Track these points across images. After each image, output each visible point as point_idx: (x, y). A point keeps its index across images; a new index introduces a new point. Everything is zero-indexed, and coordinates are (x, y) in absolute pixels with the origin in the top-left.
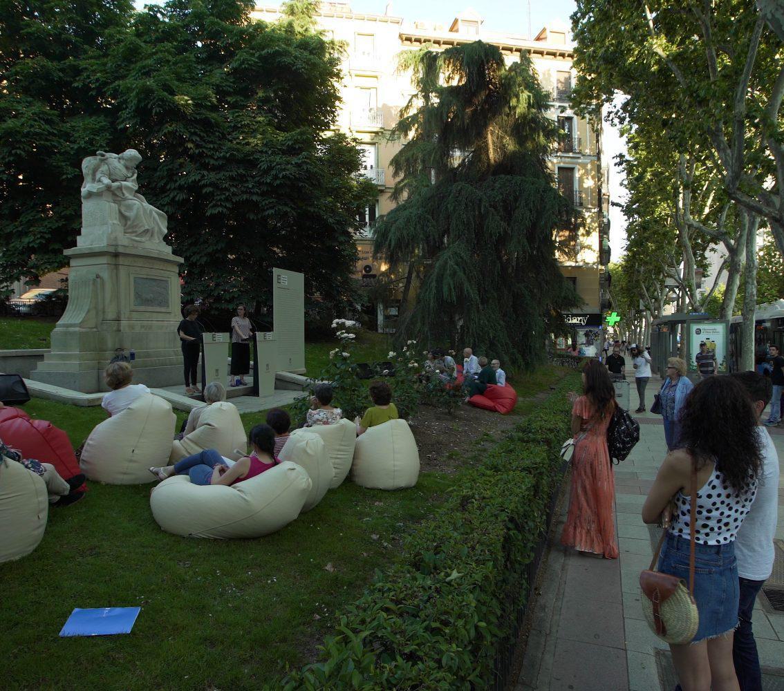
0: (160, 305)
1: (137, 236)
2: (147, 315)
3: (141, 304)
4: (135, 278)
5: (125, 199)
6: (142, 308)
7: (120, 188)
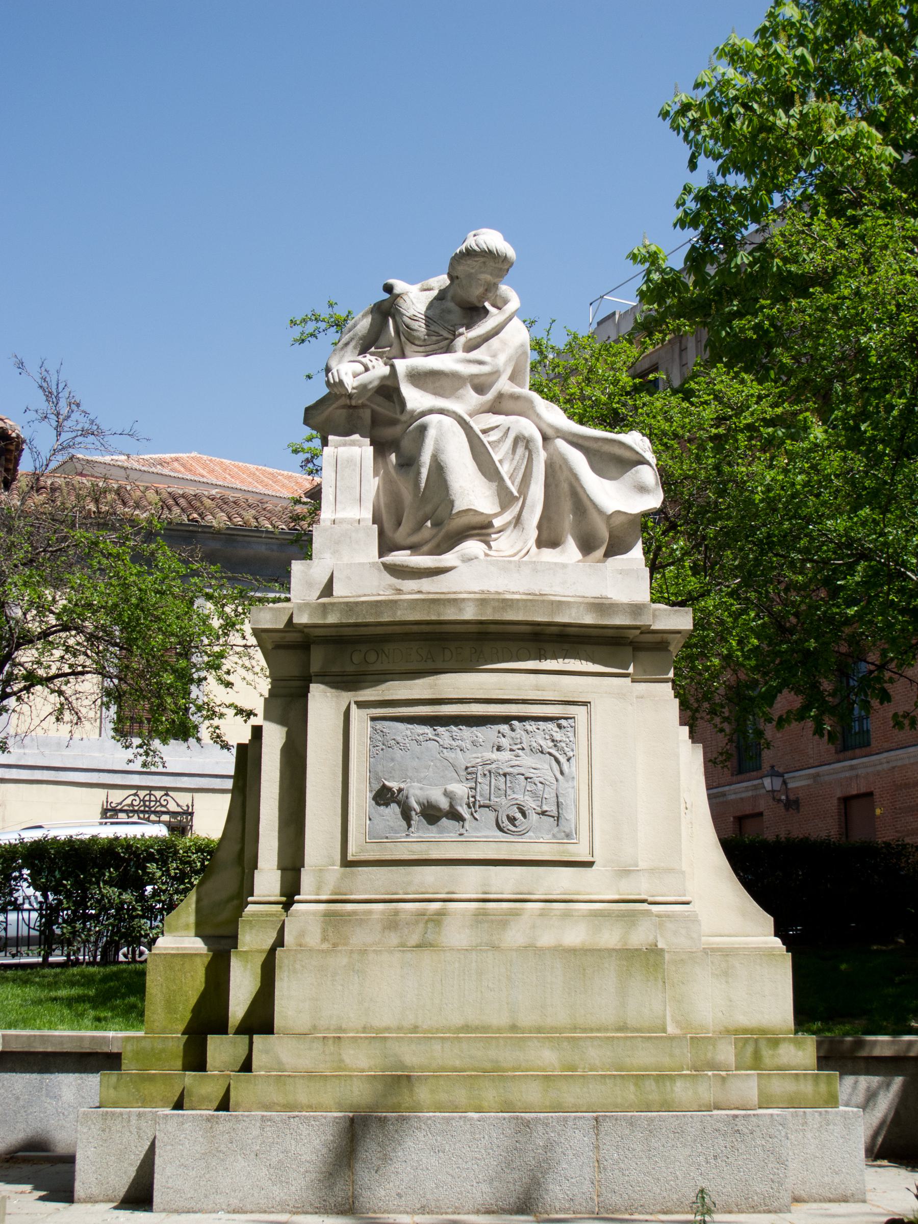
7: (388, 391)
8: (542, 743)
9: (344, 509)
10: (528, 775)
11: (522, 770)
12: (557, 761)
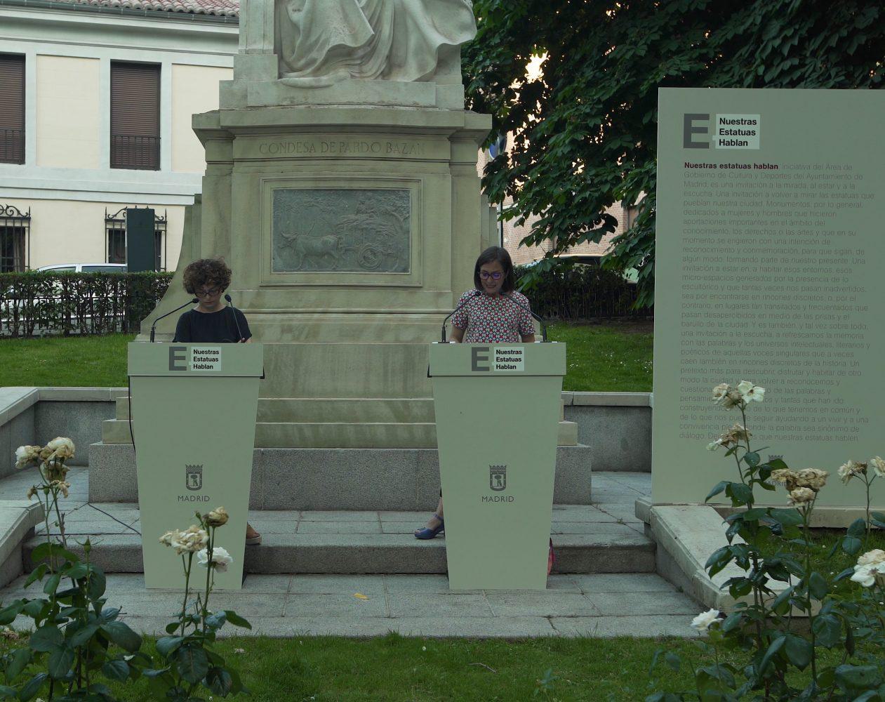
0: (365, 264)
2: (312, 295)
3: (291, 267)
4: (275, 191)
6: (297, 277)
8: (388, 208)
9: (255, 42)
10: (379, 230)
11: (375, 226)
12: (397, 218)
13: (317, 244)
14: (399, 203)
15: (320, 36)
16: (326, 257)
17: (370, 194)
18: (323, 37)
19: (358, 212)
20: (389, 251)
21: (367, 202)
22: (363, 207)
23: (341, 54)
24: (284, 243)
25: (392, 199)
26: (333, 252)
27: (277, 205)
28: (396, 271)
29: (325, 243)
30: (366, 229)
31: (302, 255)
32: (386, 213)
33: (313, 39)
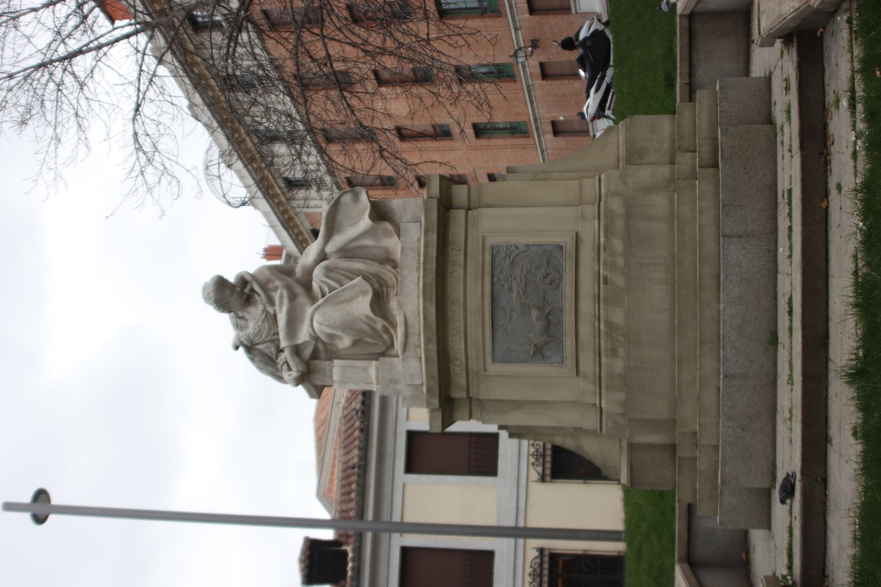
0: (556, 283)
1: (394, 325)
3: (560, 349)
4: (494, 362)
5: (316, 339)
6: (569, 343)
7: (297, 351)
8: (507, 263)
11: (523, 275)
12: (517, 255)
13: (539, 325)
14: (503, 254)
15: (364, 322)
16: (550, 318)
17: (495, 280)
18: (365, 319)
19: (510, 289)
20: (545, 262)
21: (502, 282)
22: (506, 286)
23: (379, 302)
24: (538, 353)
25: (501, 260)
26: (547, 312)
27: (506, 360)
28: (562, 256)
29: (538, 319)
30: (525, 283)
31: (549, 339)
32: (512, 264)
33: (366, 328)
